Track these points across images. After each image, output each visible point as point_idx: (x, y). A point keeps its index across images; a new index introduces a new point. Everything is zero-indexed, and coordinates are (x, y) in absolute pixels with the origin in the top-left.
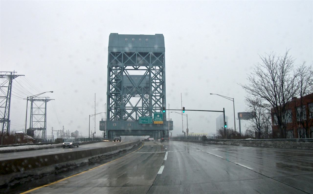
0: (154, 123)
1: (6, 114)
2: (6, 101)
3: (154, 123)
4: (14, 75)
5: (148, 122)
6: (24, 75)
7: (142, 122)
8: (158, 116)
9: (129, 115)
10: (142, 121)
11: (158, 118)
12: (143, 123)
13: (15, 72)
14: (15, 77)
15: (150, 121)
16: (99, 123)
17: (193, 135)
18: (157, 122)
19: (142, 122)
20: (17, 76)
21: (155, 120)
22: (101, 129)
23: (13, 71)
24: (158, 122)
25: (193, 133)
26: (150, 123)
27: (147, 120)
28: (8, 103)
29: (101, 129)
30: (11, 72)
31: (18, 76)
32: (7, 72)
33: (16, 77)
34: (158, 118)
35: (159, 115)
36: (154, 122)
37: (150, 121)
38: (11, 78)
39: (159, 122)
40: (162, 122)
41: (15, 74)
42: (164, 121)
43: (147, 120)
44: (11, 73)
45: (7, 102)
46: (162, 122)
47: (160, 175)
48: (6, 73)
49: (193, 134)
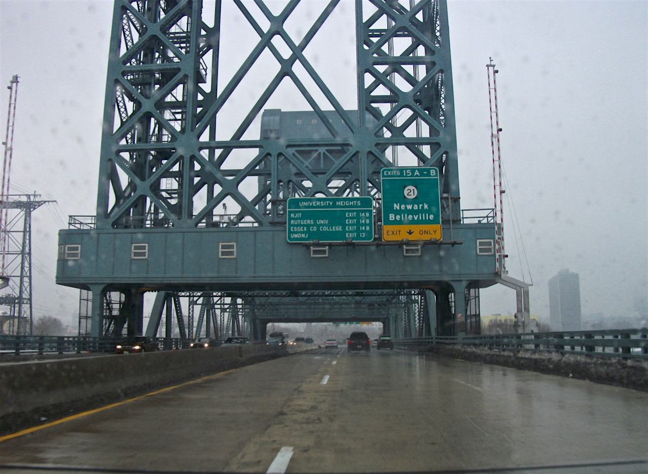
0: (386, 237)
1: (28, 289)
2: (20, 261)
3: (386, 237)
4: (35, 202)
5: (344, 232)
6: (55, 201)
7: (308, 232)
8: (411, 192)
9: (247, 208)
10: (308, 226)
11: (409, 207)
12: (311, 235)
13: (36, 194)
14: (35, 206)
15: (358, 224)
16: (56, 239)
17: (500, 321)
18: (405, 228)
19: (308, 232)
20: (40, 204)
21: (392, 217)
22: (65, 278)
23: (33, 193)
24: (410, 233)
25: (499, 315)
26: (358, 237)
27: (339, 218)
28: (27, 264)
29: (65, 278)
30: (29, 195)
31: (42, 204)
32: (20, 195)
33: (39, 206)
34: (409, 207)
35: (415, 183)
36: (386, 228)
37: (358, 224)
38: (30, 209)
39: (420, 233)
40: (438, 227)
41: (37, 199)
42: (446, 222)
43: (339, 218)
44: (29, 198)
45: (23, 263)
46: (435, 232)
47: (258, 224)
48: (18, 196)
49: (499, 318)
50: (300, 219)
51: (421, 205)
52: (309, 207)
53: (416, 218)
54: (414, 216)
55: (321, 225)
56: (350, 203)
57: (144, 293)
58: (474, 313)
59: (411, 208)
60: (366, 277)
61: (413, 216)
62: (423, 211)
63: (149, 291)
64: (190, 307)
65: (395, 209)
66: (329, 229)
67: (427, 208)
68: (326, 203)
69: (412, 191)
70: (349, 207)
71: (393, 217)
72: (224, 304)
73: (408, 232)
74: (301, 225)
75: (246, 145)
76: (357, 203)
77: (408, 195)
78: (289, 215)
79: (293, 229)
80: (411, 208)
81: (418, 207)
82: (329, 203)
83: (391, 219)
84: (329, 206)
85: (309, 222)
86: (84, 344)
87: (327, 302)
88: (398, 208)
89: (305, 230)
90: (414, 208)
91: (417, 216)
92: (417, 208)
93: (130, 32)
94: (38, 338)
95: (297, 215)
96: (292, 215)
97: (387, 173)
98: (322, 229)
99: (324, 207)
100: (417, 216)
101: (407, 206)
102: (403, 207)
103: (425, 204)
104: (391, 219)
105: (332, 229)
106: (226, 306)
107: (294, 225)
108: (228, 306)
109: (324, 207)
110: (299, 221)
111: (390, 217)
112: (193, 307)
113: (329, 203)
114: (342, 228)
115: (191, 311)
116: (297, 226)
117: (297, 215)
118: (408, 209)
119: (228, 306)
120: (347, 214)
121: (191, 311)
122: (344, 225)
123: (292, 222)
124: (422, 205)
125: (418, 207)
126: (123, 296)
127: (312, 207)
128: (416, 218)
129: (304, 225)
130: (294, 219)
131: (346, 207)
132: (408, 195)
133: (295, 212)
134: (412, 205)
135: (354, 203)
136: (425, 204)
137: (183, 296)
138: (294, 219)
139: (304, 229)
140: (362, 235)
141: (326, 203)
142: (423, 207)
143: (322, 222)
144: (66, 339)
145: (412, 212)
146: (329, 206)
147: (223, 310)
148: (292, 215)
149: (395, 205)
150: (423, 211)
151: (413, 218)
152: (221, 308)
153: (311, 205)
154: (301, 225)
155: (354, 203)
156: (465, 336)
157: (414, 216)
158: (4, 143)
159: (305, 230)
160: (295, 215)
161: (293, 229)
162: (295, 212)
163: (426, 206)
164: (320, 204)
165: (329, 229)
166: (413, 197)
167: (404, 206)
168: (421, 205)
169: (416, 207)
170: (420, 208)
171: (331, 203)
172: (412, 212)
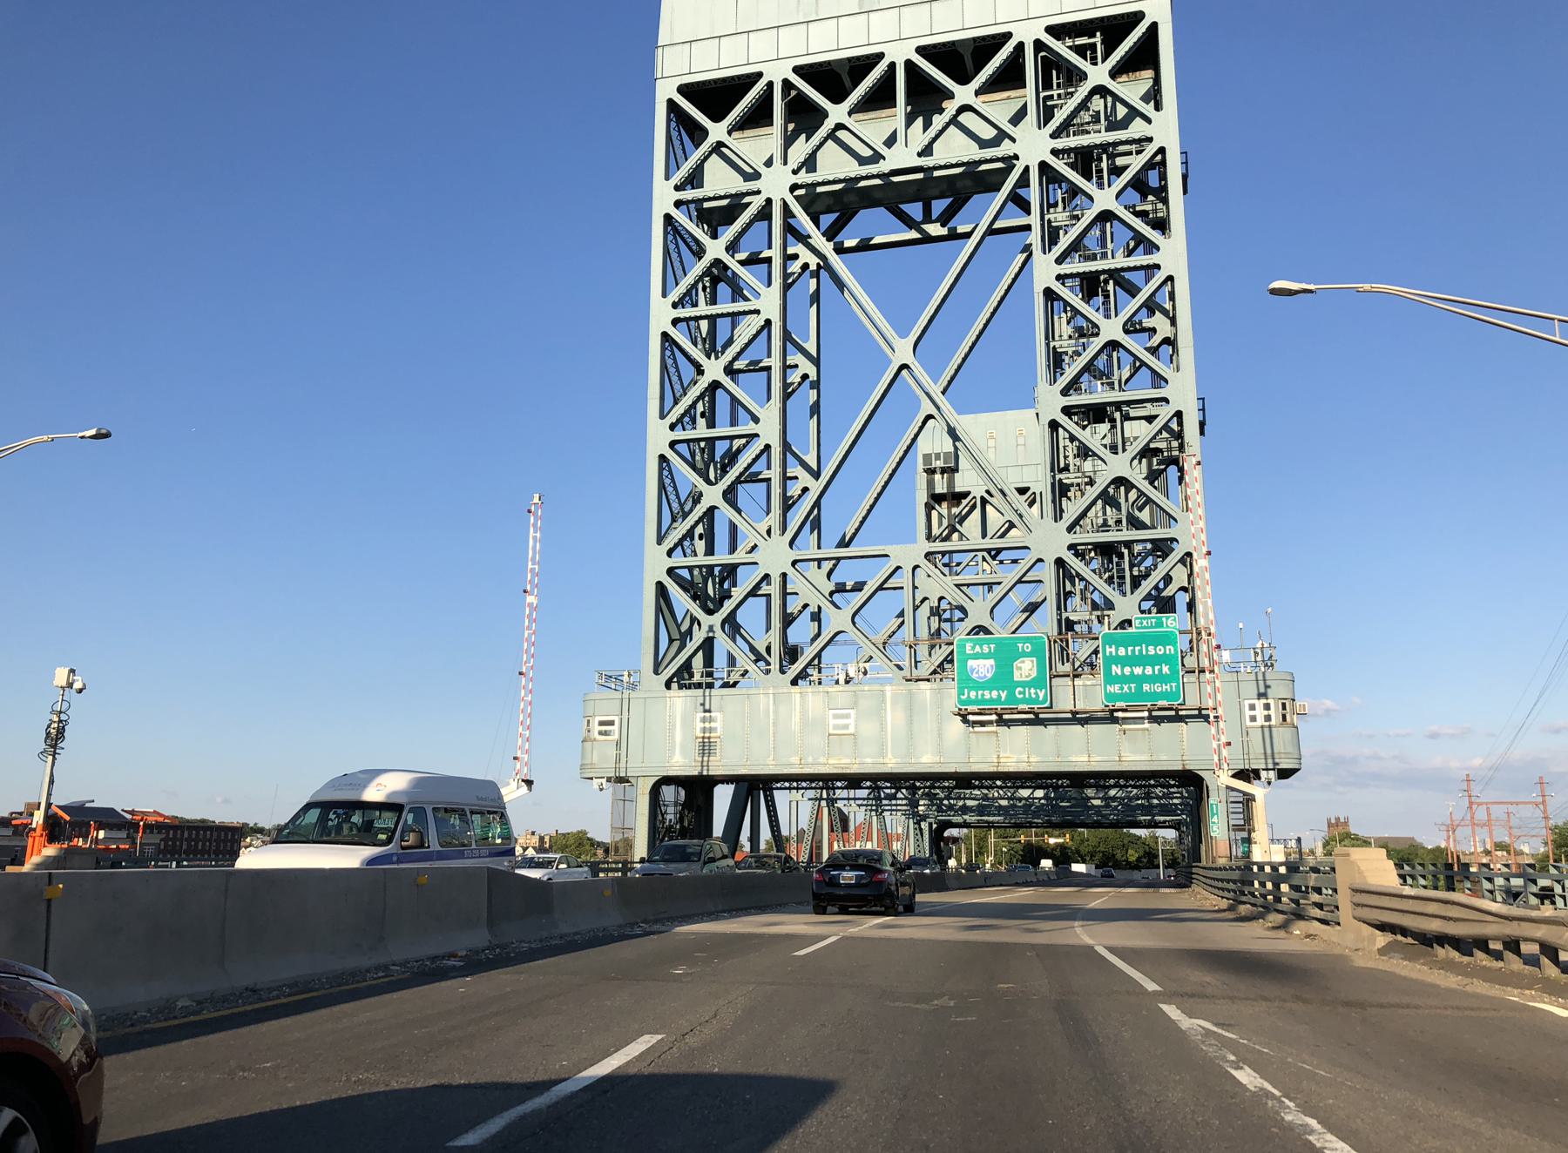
54: (1001, 692)
56: (1164, 687)
57: (715, 786)
58: (1055, 303)
59: (1140, 673)
61: (998, 691)
63: (723, 783)
65: (1114, 673)
67: (1168, 673)
73: (884, 159)
75: (1132, 720)
80: (1140, 673)
81: (1154, 671)
88: (1120, 673)
90: (1146, 672)
91: (1043, 690)
93: (675, 359)
97: (1141, 623)
100: (1043, 690)
103: (1163, 665)
118: (1136, 673)
125: (1154, 671)
126: (682, 793)
134: (1142, 667)
135: (1171, 687)
136: (1163, 665)
142: (1160, 670)
149: (1114, 667)
155: (1171, 687)
156: (1078, 597)
157: (1038, 691)
158: (1269, 687)
168: (1157, 668)
171: (1003, 696)
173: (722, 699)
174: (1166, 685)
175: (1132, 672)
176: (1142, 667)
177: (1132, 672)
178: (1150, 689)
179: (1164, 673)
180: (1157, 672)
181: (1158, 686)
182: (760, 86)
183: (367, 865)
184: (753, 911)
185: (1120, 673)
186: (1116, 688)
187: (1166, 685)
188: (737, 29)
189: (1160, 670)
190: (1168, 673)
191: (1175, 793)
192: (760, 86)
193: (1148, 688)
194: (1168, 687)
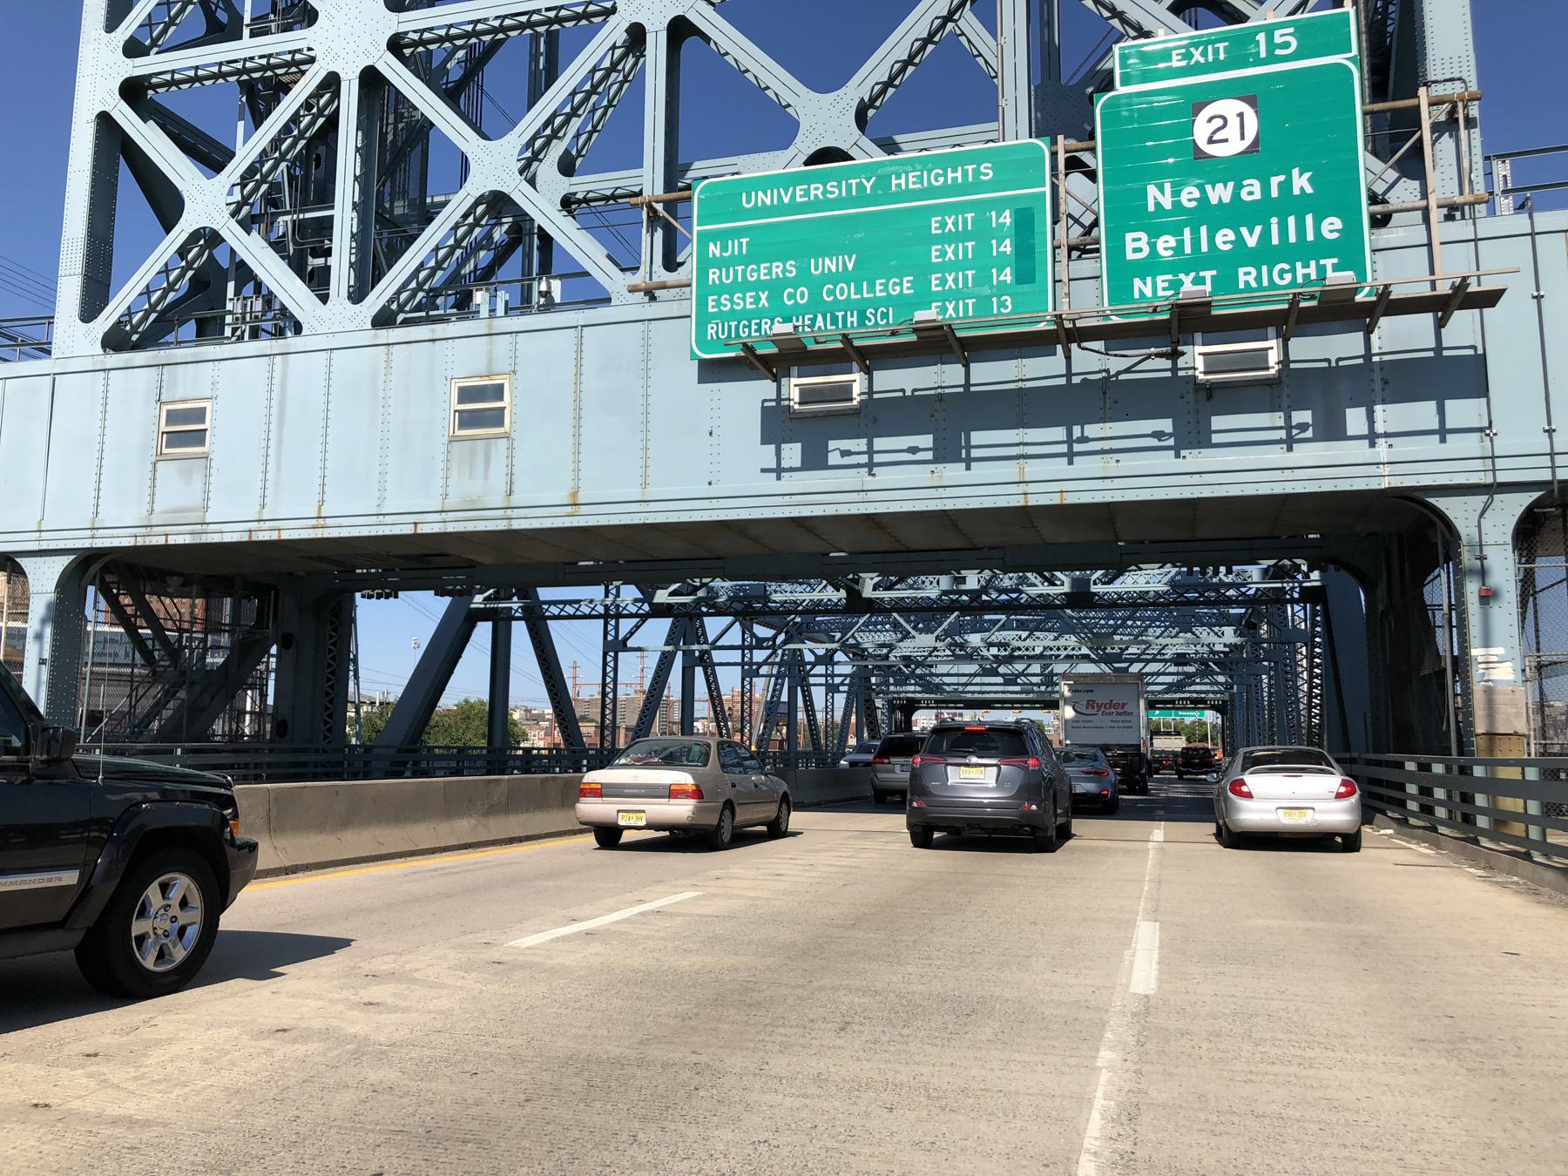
10: (775, 287)
11: (1220, 193)
34: (1220, 193)
50: (745, 260)
51: (1275, 181)
52: (780, 209)
53: (1251, 241)
54: (1244, 231)
55: (833, 278)
60: (1022, 488)
62: (1289, 204)
64: (746, 683)
66: (859, 290)
67: (1309, 190)
68: (849, 187)
69: (1234, 123)
70: (945, 191)
71: (1143, 244)
72: (833, 676)
74: (745, 286)
76: (977, 172)
77: (1211, 141)
78: (703, 250)
79: (718, 303)
81: (1266, 189)
82: (861, 186)
83: (1130, 256)
84: (862, 199)
85: (777, 269)
86: (528, 762)
87: (1065, 653)
89: (764, 301)
91: (1258, 229)
92: (1257, 196)
94: (455, 751)
95: (733, 248)
96: (714, 250)
98: (831, 292)
99: (839, 203)
100: (1258, 229)
101: (1208, 187)
102: (1189, 195)
103: (1295, 172)
104: (1130, 256)
105: (871, 288)
106: (838, 680)
107: (719, 289)
108: (842, 678)
109: (839, 203)
110: (740, 268)
111: (1130, 245)
112: (833, 697)
113: (861, 186)
114: (913, 284)
115: (830, 709)
116: (731, 290)
117: (733, 248)
118: (1214, 201)
119: (842, 678)
120: (934, 222)
121: (830, 709)
122: (922, 271)
123: (713, 275)
124: (1282, 178)
125: (1266, 189)
127: (794, 208)
128: (1251, 241)
129: (759, 286)
130: (720, 263)
131: (930, 192)
132: (1211, 141)
133: (723, 237)
134: (1231, 185)
135: (965, 173)
136: (1295, 172)
137: (555, 617)
138: (720, 263)
139: (757, 299)
140: (1002, 305)
141: (849, 187)
142: (1286, 186)
143: (831, 264)
144: (535, 752)
145: (1236, 214)
146: (862, 199)
147: (832, 689)
148: (714, 250)
150: (1289, 204)
151: (1240, 240)
152: (826, 685)
153: (786, 200)
154: (745, 286)
155: (965, 173)
157: (1244, 231)
159: (764, 301)
160: (724, 248)
161: (718, 303)
162: (723, 237)
163: (1301, 182)
164: (825, 192)
165: (859, 290)
166: (1235, 146)
167: (1231, 236)
168: (1275, 181)
169: (1252, 190)
170: (1274, 193)
172: (1236, 214)
173: (575, 494)
174: (1306, 266)
175: (1204, 199)
176: (1231, 185)
177: (1204, 199)
178: (1258, 279)
179: (1296, 192)
180: (1274, 193)
181: (1282, 272)
182: (378, 298)
183: (143, 901)
184: (486, 559)
185: (1167, 205)
186: (1160, 285)
187: (1306, 266)
188: (382, 499)
189: (1286, 186)
190: (1309, 190)
191: (1158, 674)
192: (378, 298)
193: (1251, 279)
194: (959, 174)
